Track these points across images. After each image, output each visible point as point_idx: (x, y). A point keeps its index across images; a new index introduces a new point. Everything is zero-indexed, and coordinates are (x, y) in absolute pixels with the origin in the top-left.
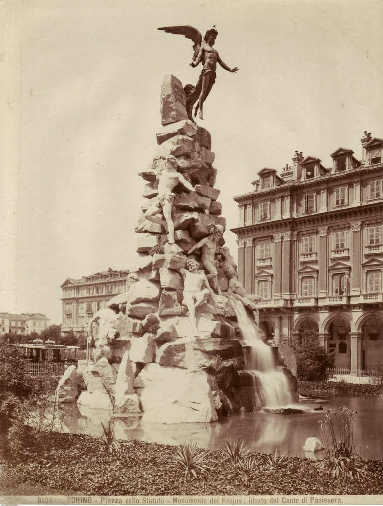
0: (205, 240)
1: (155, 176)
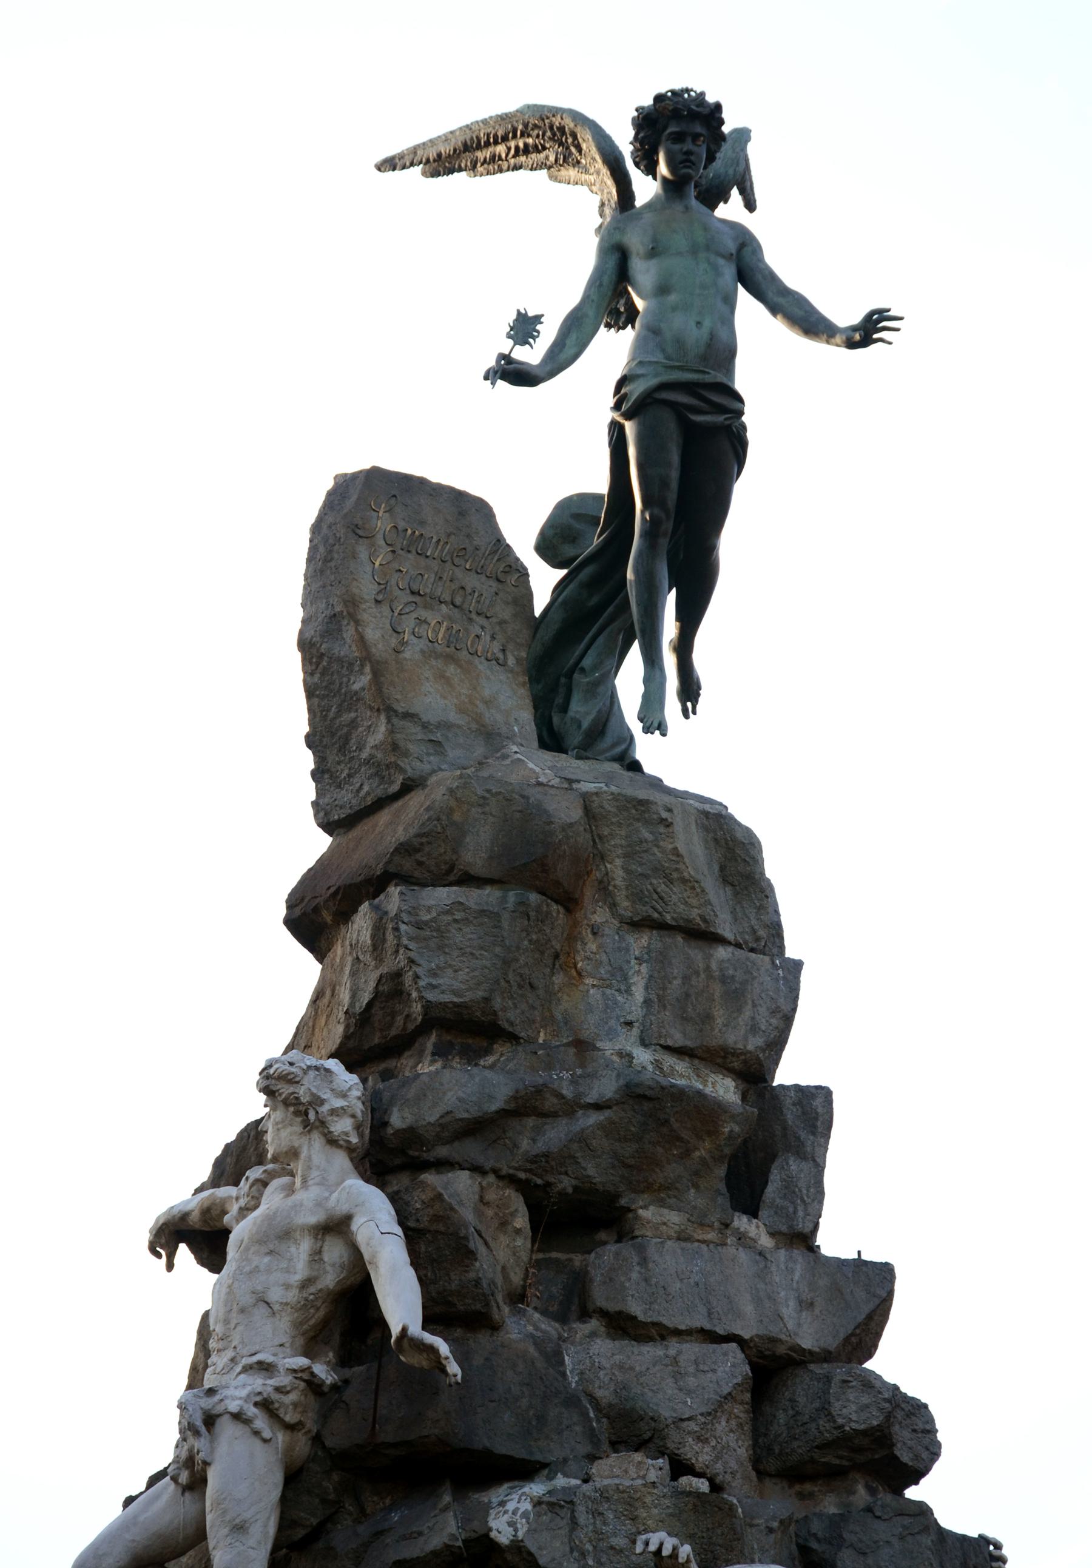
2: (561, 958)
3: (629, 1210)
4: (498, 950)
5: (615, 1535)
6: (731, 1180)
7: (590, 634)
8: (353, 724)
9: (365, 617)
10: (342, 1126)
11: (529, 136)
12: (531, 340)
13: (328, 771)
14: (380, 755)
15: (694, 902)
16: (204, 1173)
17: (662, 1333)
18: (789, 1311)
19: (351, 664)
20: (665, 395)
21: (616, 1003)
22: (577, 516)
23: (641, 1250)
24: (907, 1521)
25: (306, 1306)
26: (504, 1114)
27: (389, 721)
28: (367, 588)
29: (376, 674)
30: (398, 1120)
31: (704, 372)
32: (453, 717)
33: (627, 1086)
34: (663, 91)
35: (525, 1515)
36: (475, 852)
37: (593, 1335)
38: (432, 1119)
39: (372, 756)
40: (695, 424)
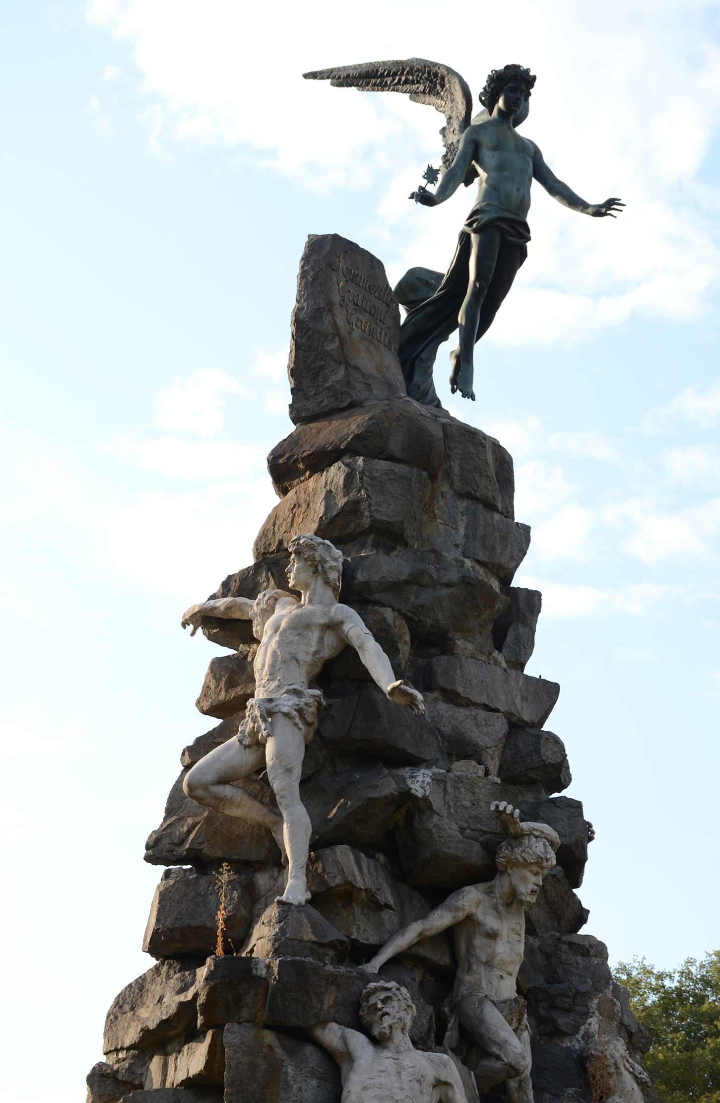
0: (471, 899)
1: (250, 622)
2: (428, 508)
3: (452, 639)
4: (409, 497)
5: (465, 800)
6: (494, 632)
7: (427, 341)
8: (322, 368)
9: (336, 312)
10: (334, 576)
11: (412, 75)
13: (302, 390)
14: (338, 386)
15: (490, 488)
16: (216, 588)
17: (468, 703)
18: (518, 700)
19: (326, 336)
20: (498, 223)
21: (451, 534)
22: (419, 279)
23: (460, 660)
24: (572, 810)
25: (313, 664)
26: (407, 582)
27: (346, 369)
28: (336, 298)
29: (342, 343)
30: (361, 576)
32: (375, 372)
33: (463, 577)
35: (428, 784)
36: (396, 443)
37: (436, 700)
38: (377, 579)
39: (332, 386)
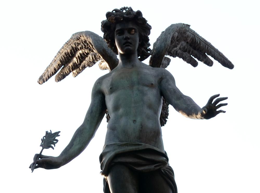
12: (53, 145)
20: (120, 160)
31: (139, 145)
34: (111, 11)
40: (141, 172)
